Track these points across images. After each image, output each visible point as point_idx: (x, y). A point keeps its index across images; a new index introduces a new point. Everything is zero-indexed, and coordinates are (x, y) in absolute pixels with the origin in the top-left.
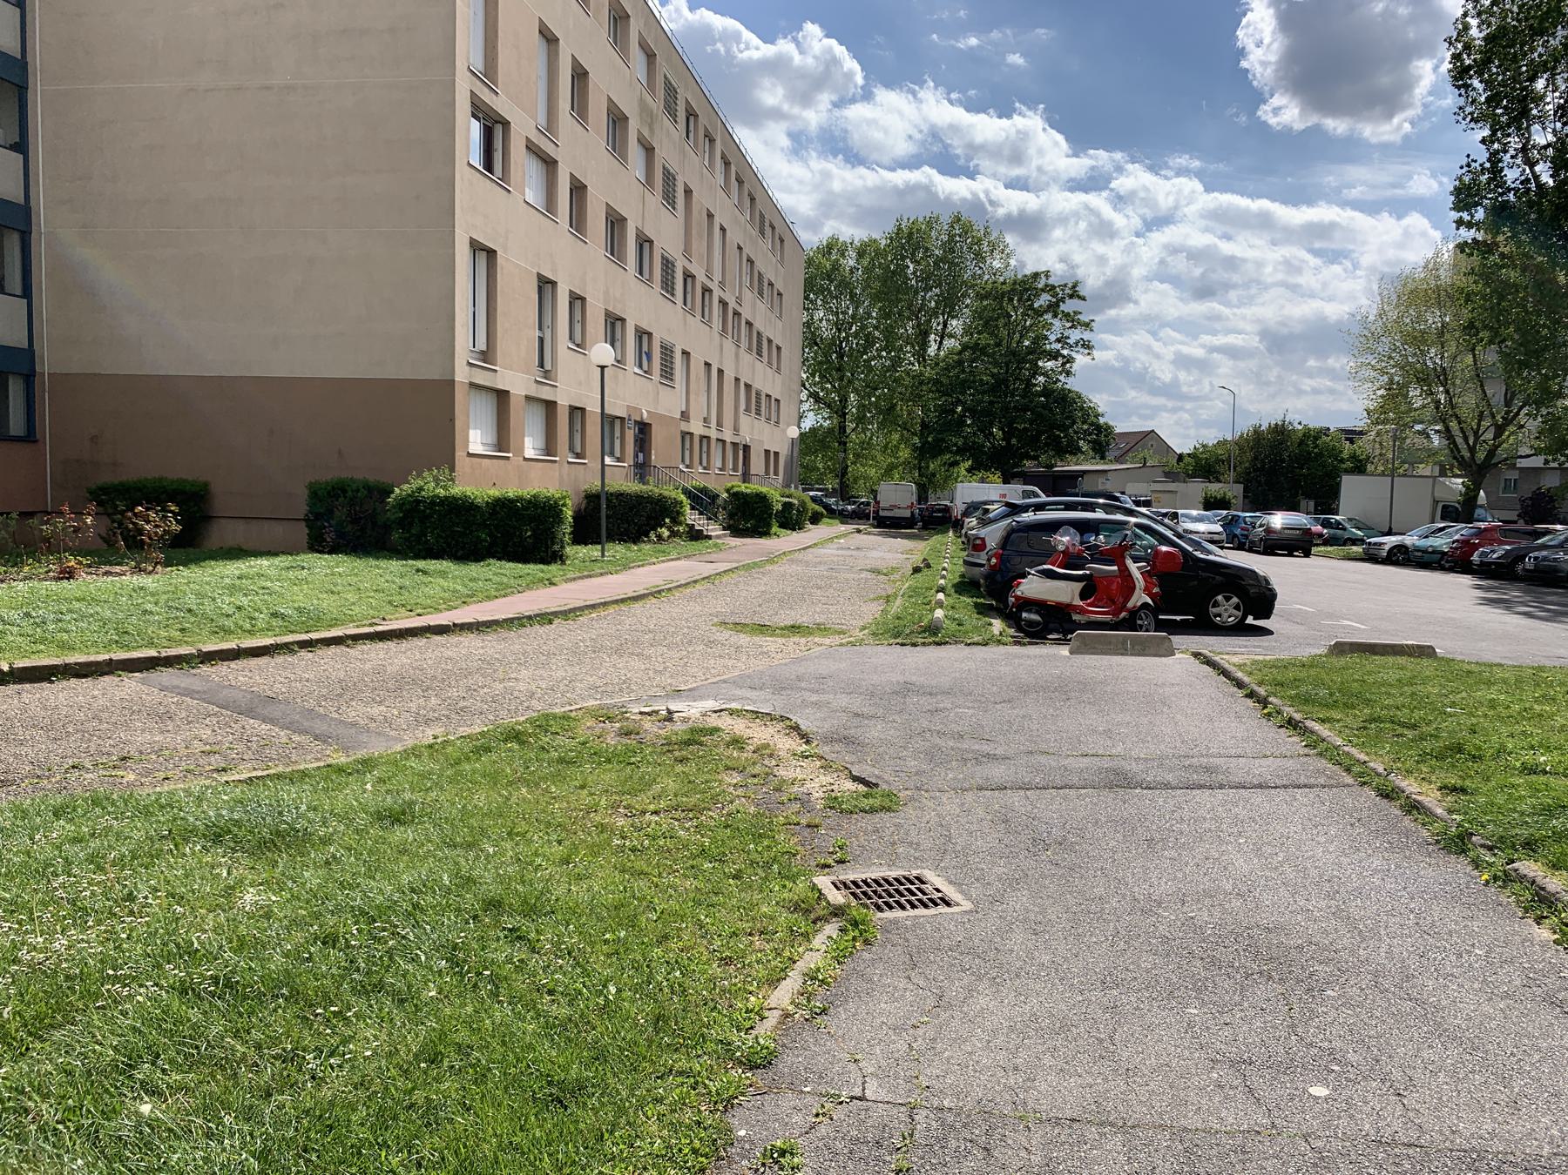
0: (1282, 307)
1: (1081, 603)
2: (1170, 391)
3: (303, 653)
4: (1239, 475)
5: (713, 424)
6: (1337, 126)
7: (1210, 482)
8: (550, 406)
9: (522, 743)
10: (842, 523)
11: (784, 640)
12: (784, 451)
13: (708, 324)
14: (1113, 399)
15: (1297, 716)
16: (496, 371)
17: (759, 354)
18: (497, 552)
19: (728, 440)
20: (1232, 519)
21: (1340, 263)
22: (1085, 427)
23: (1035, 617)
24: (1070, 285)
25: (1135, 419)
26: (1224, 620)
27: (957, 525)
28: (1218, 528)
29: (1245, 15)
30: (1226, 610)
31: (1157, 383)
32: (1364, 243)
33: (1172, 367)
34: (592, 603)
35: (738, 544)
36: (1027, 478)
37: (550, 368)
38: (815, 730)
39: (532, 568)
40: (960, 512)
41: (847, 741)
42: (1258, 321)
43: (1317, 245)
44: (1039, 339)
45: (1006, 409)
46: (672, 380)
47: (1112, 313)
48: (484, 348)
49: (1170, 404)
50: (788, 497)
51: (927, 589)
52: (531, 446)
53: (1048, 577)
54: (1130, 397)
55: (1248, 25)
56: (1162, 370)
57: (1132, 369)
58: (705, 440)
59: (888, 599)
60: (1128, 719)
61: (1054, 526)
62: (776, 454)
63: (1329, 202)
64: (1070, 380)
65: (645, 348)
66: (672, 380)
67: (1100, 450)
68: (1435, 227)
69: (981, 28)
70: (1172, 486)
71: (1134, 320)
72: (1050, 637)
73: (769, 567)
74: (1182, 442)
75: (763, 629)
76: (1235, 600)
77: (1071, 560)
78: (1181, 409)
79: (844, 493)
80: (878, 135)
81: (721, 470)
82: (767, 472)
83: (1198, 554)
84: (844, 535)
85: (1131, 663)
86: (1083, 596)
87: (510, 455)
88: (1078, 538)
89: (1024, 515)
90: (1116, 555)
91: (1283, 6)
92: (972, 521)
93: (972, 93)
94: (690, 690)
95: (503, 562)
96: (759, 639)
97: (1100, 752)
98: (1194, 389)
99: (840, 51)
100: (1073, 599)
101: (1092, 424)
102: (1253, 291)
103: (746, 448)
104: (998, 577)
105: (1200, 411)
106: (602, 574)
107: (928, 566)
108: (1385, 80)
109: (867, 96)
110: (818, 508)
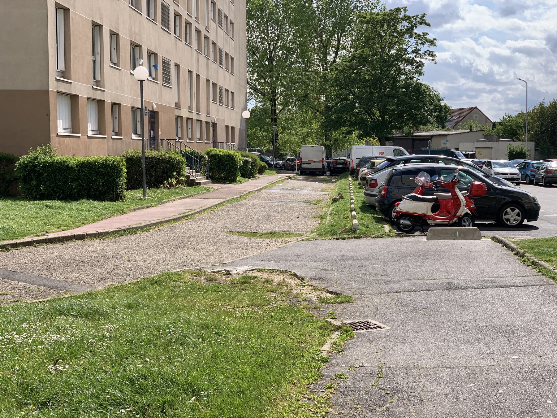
1: (432, 214)
2: (488, 79)
3: (13, 250)
4: (532, 135)
5: (194, 111)
7: (513, 141)
8: (100, 103)
9: (160, 285)
10: (278, 173)
11: (269, 240)
12: (237, 124)
13: (189, 45)
14: (450, 85)
15: (536, 260)
16: (71, 83)
17: (221, 63)
18: (82, 195)
19: (204, 121)
20: (525, 165)
22: (432, 107)
23: (407, 222)
24: (420, 16)
25: (464, 98)
26: (511, 222)
27: (354, 173)
28: (516, 171)
30: (512, 216)
31: (479, 74)
33: (488, 63)
34: (154, 222)
35: (219, 187)
36: (396, 141)
37: (100, 79)
38: (304, 275)
39: (107, 204)
40: (355, 165)
41: (320, 279)
42: (545, 31)
44: (401, 51)
45: (381, 97)
46: (169, 83)
47: (447, 26)
48: (63, 69)
49: (488, 88)
50: (245, 156)
51: (344, 210)
52: (91, 129)
53: (414, 200)
54: (461, 84)
56: (482, 65)
57: (462, 64)
58: (179, 119)
59: (321, 218)
60: (456, 265)
61: (416, 172)
62: (233, 128)
64: (421, 78)
65: (153, 63)
66: (169, 83)
67: (441, 122)
70: (489, 144)
71: (462, 31)
72: (416, 233)
73: (242, 201)
74: (495, 116)
75: (253, 234)
76: (517, 211)
77: (425, 190)
78: (495, 91)
79: (277, 153)
81: (199, 140)
83: (496, 186)
84: (282, 181)
85: (458, 243)
86: (434, 210)
87: (80, 135)
88: (429, 178)
89: (398, 166)
90: (450, 187)
92: (364, 170)
94: (230, 263)
95: (91, 201)
96: (254, 239)
97: (442, 278)
98: (503, 77)
100: (427, 212)
101: (436, 105)
102: (541, 10)
103: (215, 125)
104: (386, 202)
105: (508, 92)
106: (148, 207)
107: (342, 198)
110: (262, 163)
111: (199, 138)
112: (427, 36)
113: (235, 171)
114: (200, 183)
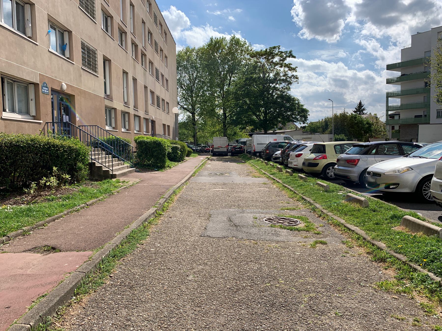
0: (307, 88)
6: (320, 38)
19: (142, 116)
21: (322, 76)
29: (293, 6)
32: (328, 70)
43: (316, 71)
46: (96, 72)
50: (174, 144)
55: (294, 9)
62: (168, 126)
63: (318, 60)
64: (289, 92)
68: (346, 66)
69: (221, 9)
79: (196, 143)
80: (195, 40)
81: (139, 131)
82: (165, 134)
91: (304, 4)
93: (220, 27)
99: (182, 14)
103: (153, 122)
108: (332, 25)
109: (190, 29)
110: (188, 149)
111: (138, 130)
112: (291, 66)
113: (163, 158)
114: (115, 175)
